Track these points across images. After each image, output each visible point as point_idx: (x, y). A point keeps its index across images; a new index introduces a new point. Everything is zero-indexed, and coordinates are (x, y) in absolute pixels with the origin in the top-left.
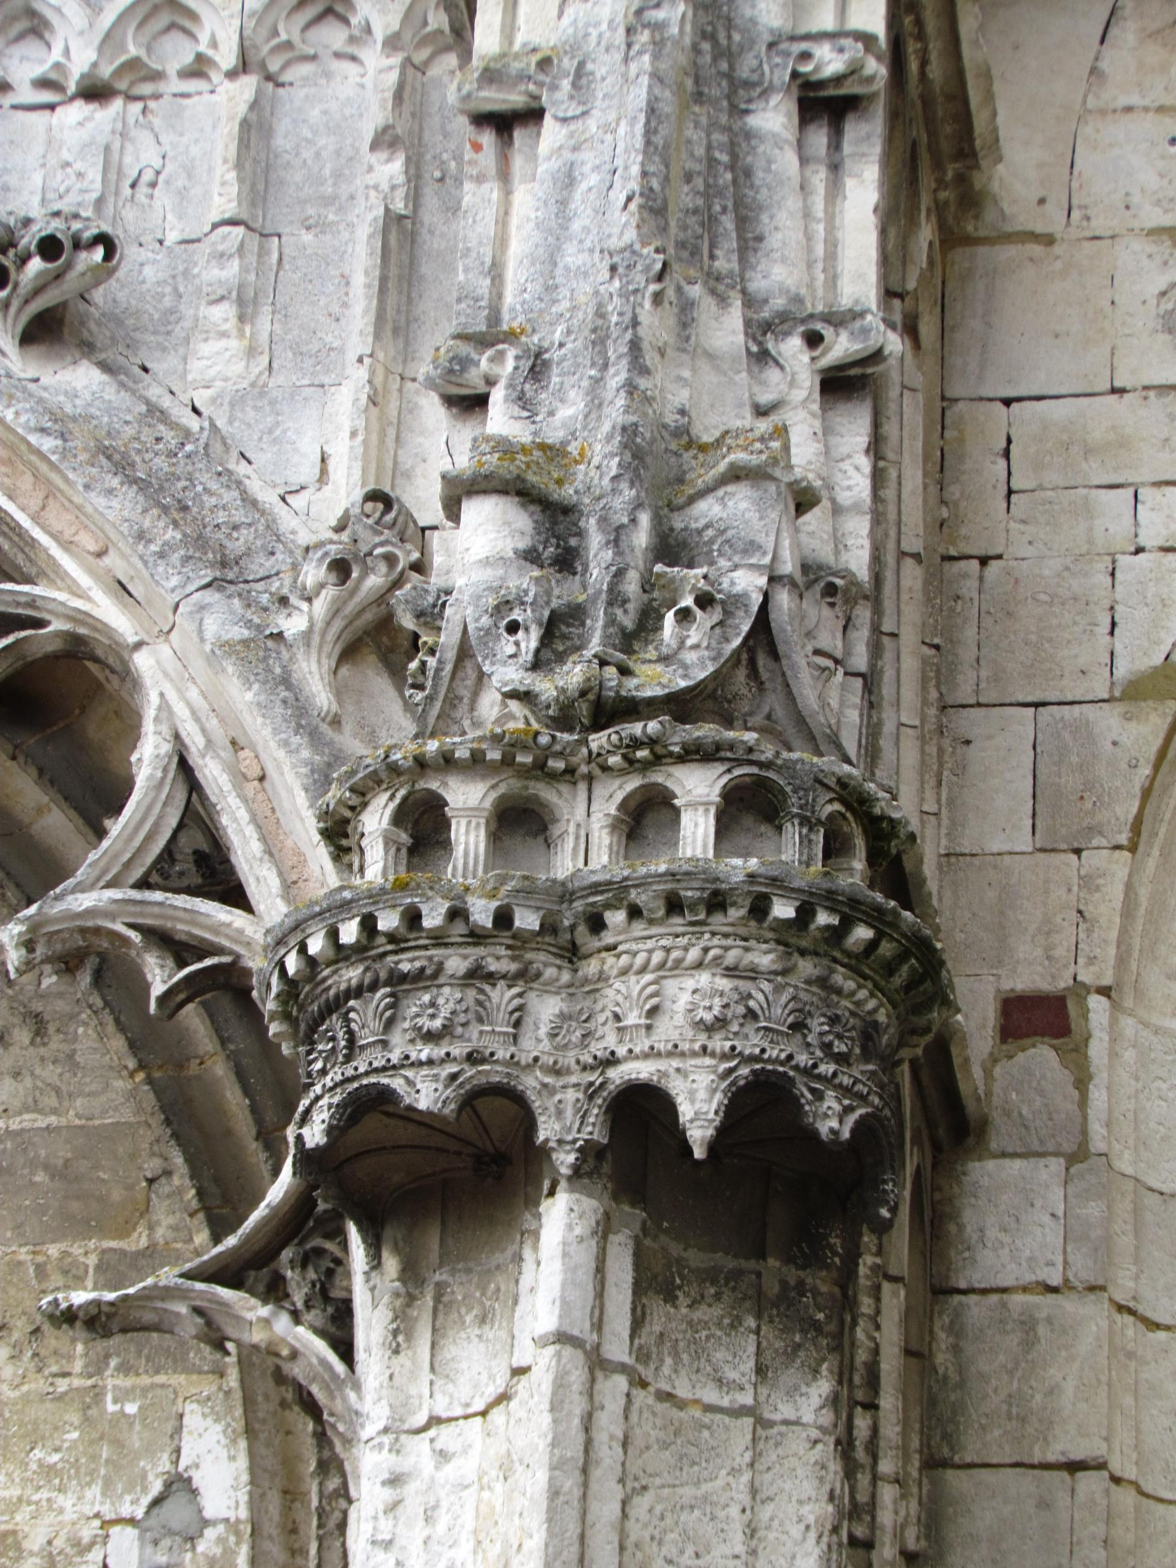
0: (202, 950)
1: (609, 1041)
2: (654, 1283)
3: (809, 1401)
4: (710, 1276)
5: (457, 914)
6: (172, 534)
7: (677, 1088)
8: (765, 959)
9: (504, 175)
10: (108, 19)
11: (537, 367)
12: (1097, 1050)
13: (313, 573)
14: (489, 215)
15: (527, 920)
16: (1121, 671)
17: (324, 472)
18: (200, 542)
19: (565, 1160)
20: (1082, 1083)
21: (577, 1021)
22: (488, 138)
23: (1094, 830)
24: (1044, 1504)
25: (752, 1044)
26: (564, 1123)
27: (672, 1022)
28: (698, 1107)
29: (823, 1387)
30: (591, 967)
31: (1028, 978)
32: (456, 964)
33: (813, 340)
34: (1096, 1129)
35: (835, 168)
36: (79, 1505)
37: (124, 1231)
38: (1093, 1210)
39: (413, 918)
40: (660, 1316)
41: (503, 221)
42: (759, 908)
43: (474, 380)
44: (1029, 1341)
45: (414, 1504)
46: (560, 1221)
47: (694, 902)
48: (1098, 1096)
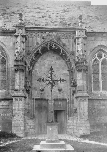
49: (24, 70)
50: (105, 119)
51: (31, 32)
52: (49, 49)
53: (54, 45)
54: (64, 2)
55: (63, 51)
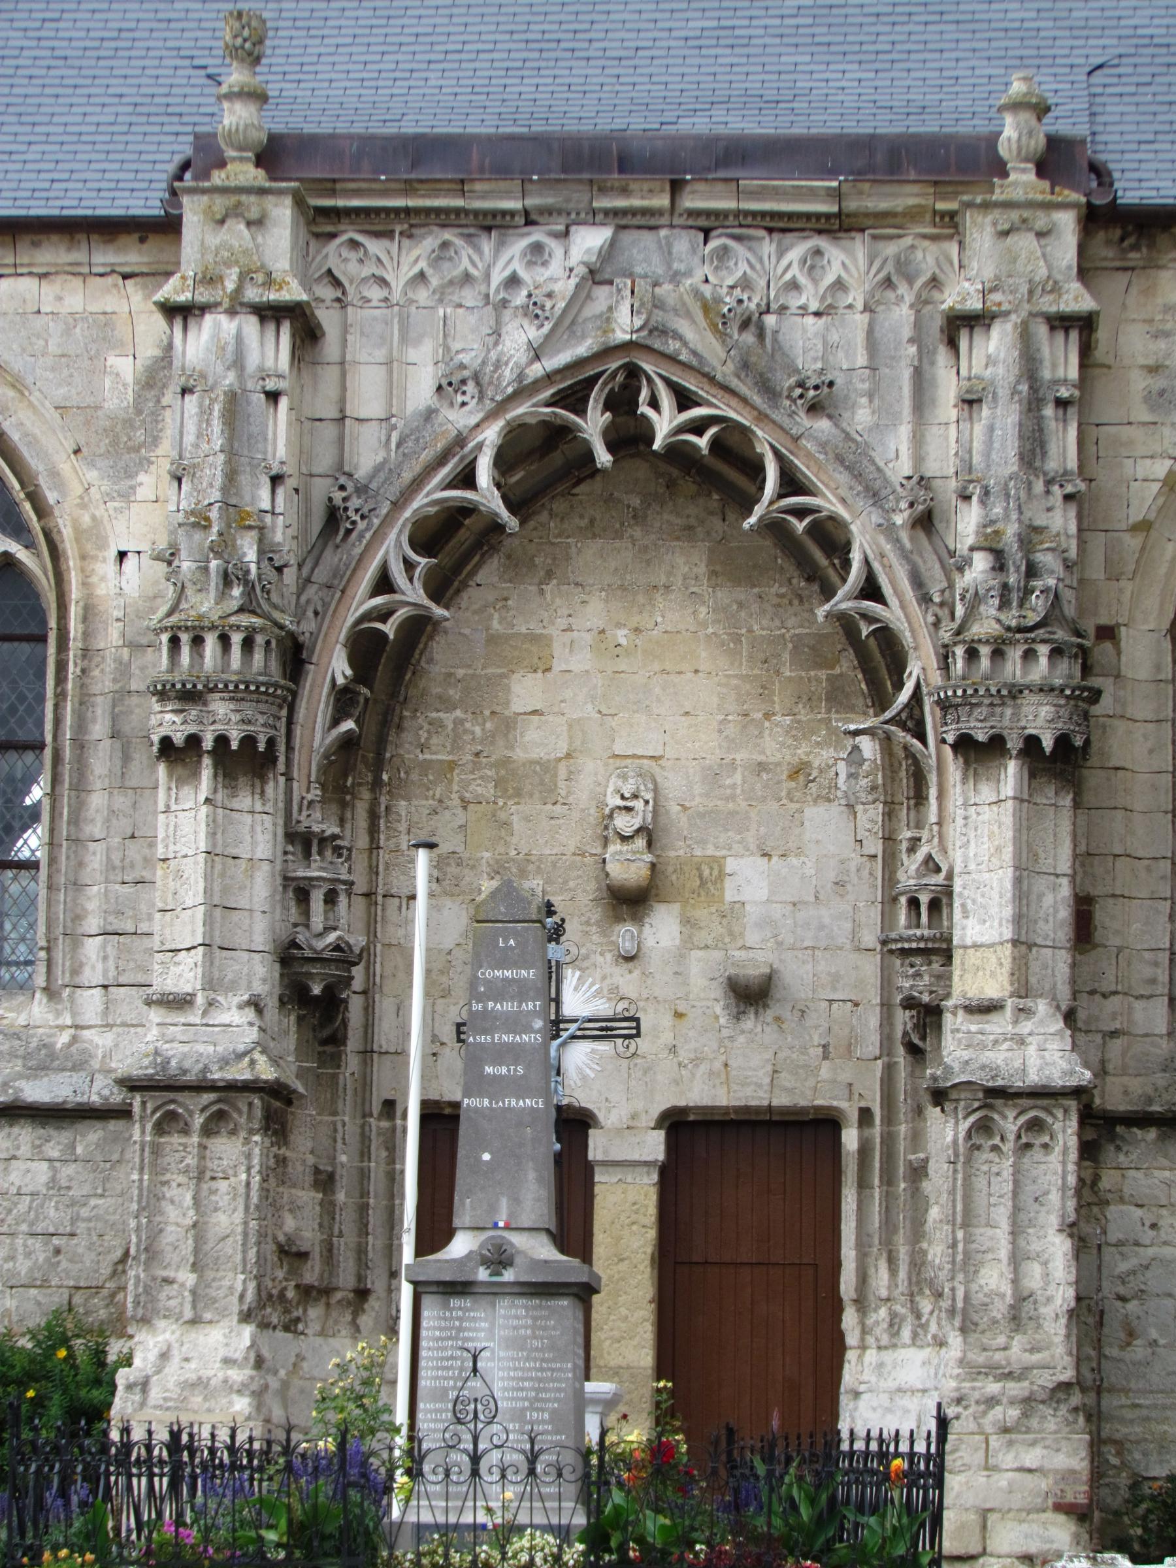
0: (877, 620)
1: (1023, 723)
2: (1032, 775)
3: (1067, 801)
4: (1044, 770)
5: (988, 690)
6: (860, 488)
7: (1042, 737)
8: (1062, 702)
9: (971, 418)
10: (821, 291)
11: (986, 493)
12: (1123, 644)
13: (903, 505)
14: (967, 433)
15: (1004, 692)
16: (1131, 521)
17: (897, 457)
18: (867, 488)
19: (1014, 752)
20: (1119, 654)
21: (1016, 715)
22: (966, 407)
23: (1122, 573)
24: (1109, 779)
25: (1060, 725)
26: (1014, 743)
27: (1041, 719)
28: (1048, 743)
29: (1071, 796)
30: (1019, 701)
31: (1104, 620)
32: (987, 701)
33: (1061, 486)
34: (1123, 668)
35: (1065, 421)
36: (827, 754)
37: (833, 668)
38: (1121, 693)
39: (976, 691)
40: (1035, 783)
41: (971, 434)
42: (1062, 691)
43: (968, 493)
44: (1104, 732)
45: (971, 825)
46: (1012, 766)
47: (1045, 689)
48: (1123, 659)
49: (271, 742)
50: (789, 1566)
51: (378, 235)
52: (603, 457)
53: (666, 400)
54: (298, 341)
55: (791, 483)
